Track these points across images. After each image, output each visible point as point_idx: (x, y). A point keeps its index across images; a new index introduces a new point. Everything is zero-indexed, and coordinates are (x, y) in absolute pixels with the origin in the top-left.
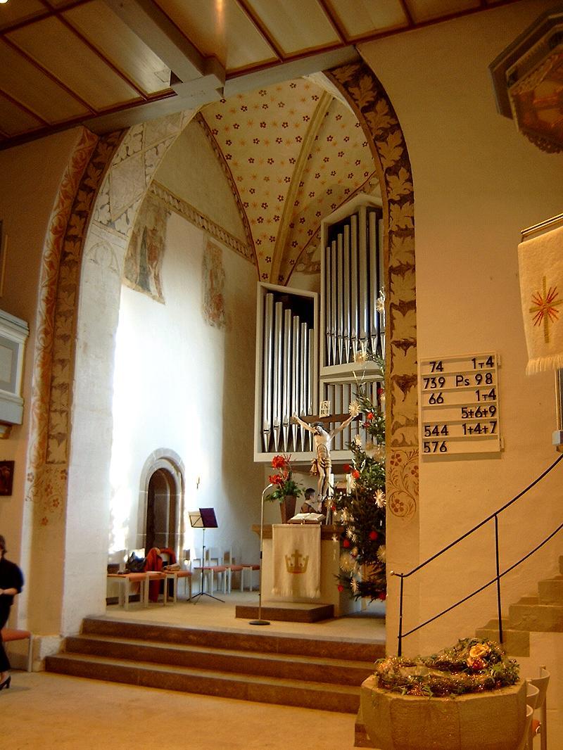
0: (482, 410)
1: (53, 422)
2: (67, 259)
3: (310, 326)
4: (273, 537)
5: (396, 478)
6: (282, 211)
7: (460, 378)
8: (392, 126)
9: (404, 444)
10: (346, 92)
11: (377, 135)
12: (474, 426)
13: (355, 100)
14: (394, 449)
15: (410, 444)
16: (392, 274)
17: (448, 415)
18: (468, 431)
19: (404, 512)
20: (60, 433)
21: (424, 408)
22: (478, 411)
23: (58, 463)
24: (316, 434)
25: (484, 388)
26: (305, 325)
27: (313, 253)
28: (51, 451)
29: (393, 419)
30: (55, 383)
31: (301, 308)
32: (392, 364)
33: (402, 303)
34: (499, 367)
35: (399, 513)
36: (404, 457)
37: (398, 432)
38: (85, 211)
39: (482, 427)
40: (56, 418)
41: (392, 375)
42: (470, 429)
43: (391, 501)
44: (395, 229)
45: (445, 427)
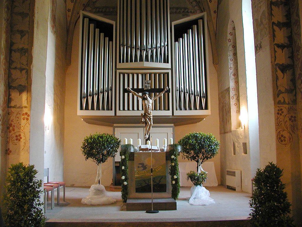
1: (13, 77)
3: (111, 39)
5: (281, 122)
14: (279, 105)
15: (287, 103)
16: (272, 5)
19: (286, 142)
20: (20, 85)
29: (277, 88)
30: (15, 47)
31: (106, 30)
32: (275, 57)
33: (279, 22)
35: (284, 143)
37: (281, 95)
40: (16, 74)
41: (276, 63)
43: (278, 136)
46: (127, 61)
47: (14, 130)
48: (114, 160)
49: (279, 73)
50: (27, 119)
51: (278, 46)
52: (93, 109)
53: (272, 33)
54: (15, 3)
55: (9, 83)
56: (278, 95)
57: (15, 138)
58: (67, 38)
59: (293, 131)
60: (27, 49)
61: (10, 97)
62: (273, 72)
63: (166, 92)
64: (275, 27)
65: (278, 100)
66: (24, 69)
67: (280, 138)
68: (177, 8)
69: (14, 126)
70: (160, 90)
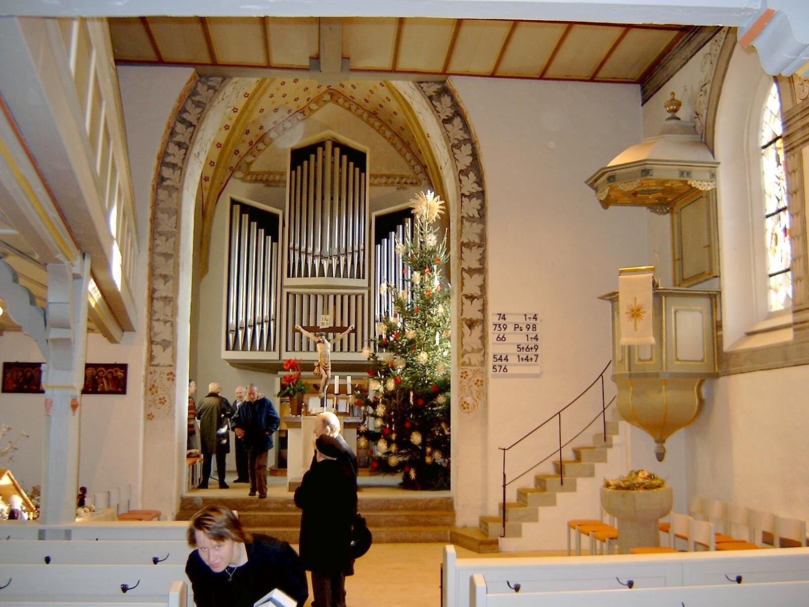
0: (529, 347)
2: (165, 183)
3: (275, 239)
4: (302, 427)
6: (233, 122)
7: (516, 326)
8: (465, 140)
9: (470, 364)
10: (430, 104)
11: (453, 143)
12: (524, 357)
13: (438, 112)
14: (463, 367)
17: (508, 349)
18: (521, 360)
20: (164, 340)
21: (493, 343)
22: (527, 348)
23: (163, 366)
24: (319, 342)
25: (531, 333)
26: (269, 238)
27: (251, 163)
28: (156, 355)
30: (156, 295)
31: (268, 223)
32: (462, 310)
33: (469, 268)
34: (541, 321)
35: (467, 410)
36: (470, 374)
37: (466, 356)
38: (185, 143)
39: (529, 358)
41: (462, 317)
42: (522, 359)
44: (465, 215)
45: (507, 356)
46: (299, 276)
47: (157, 392)
48: (532, 491)
49: (466, 328)
50: (173, 380)
51: (467, 297)
52: (244, 348)
53: (460, 281)
54: (156, 242)
55: (150, 337)
56: (463, 356)
57: (158, 401)
58: (203, 225)
59: (478, 397)
60: (172, 298)
61: (153, 354)
62: (458, 328)
63: (351, 332)
64: (464, 273)
65: (462, 360)
66: (169, 321)
67: (462, 406)
68: (388, 177)
69: (157, 388)
70: (342, 329)
